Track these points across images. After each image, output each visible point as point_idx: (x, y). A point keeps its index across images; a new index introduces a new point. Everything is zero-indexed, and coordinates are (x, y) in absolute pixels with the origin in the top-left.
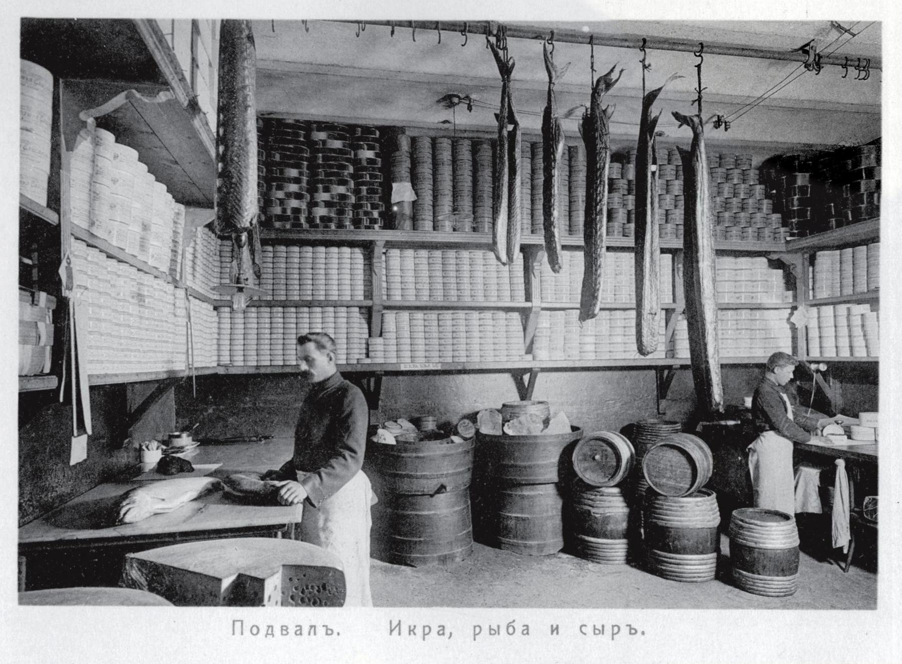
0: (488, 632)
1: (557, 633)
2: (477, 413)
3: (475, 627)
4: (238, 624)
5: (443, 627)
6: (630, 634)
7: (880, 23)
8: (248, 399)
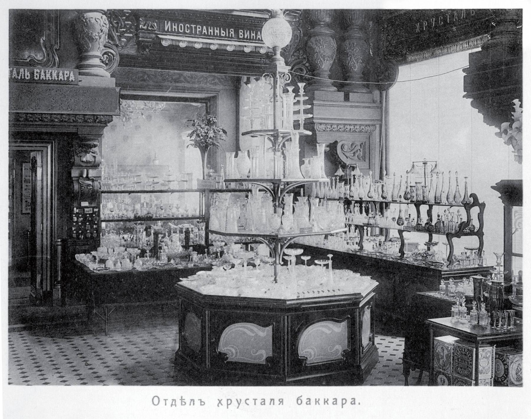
3: (342, 399)
5: (354, 399)
6: (201, 405)
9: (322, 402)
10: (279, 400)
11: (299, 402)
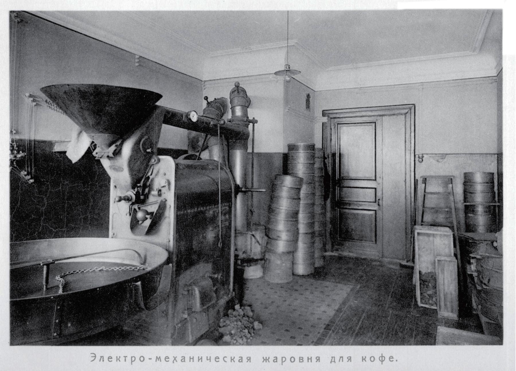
1: (231, 358)
3: (282, 358)
8: (59, 307)
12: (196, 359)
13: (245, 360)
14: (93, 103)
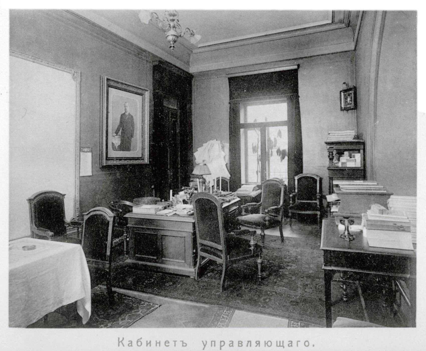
0: (237, 345)
1: (265, 342)
2: (65, 195)
3: (221, 342)
4: (213, 343)
7: (10, 326)
9: (153, 343)
10: (256, 342)
11: (139, 344)
12: (153, 343)
13: (236, 344)
14: (299, 257)
